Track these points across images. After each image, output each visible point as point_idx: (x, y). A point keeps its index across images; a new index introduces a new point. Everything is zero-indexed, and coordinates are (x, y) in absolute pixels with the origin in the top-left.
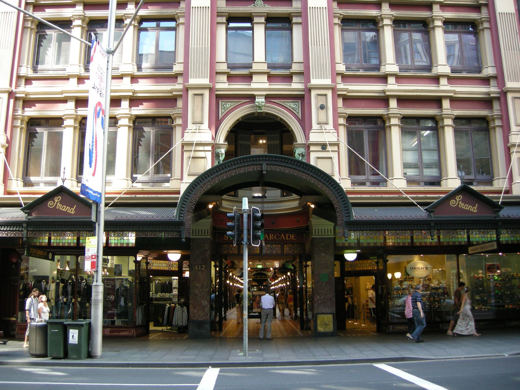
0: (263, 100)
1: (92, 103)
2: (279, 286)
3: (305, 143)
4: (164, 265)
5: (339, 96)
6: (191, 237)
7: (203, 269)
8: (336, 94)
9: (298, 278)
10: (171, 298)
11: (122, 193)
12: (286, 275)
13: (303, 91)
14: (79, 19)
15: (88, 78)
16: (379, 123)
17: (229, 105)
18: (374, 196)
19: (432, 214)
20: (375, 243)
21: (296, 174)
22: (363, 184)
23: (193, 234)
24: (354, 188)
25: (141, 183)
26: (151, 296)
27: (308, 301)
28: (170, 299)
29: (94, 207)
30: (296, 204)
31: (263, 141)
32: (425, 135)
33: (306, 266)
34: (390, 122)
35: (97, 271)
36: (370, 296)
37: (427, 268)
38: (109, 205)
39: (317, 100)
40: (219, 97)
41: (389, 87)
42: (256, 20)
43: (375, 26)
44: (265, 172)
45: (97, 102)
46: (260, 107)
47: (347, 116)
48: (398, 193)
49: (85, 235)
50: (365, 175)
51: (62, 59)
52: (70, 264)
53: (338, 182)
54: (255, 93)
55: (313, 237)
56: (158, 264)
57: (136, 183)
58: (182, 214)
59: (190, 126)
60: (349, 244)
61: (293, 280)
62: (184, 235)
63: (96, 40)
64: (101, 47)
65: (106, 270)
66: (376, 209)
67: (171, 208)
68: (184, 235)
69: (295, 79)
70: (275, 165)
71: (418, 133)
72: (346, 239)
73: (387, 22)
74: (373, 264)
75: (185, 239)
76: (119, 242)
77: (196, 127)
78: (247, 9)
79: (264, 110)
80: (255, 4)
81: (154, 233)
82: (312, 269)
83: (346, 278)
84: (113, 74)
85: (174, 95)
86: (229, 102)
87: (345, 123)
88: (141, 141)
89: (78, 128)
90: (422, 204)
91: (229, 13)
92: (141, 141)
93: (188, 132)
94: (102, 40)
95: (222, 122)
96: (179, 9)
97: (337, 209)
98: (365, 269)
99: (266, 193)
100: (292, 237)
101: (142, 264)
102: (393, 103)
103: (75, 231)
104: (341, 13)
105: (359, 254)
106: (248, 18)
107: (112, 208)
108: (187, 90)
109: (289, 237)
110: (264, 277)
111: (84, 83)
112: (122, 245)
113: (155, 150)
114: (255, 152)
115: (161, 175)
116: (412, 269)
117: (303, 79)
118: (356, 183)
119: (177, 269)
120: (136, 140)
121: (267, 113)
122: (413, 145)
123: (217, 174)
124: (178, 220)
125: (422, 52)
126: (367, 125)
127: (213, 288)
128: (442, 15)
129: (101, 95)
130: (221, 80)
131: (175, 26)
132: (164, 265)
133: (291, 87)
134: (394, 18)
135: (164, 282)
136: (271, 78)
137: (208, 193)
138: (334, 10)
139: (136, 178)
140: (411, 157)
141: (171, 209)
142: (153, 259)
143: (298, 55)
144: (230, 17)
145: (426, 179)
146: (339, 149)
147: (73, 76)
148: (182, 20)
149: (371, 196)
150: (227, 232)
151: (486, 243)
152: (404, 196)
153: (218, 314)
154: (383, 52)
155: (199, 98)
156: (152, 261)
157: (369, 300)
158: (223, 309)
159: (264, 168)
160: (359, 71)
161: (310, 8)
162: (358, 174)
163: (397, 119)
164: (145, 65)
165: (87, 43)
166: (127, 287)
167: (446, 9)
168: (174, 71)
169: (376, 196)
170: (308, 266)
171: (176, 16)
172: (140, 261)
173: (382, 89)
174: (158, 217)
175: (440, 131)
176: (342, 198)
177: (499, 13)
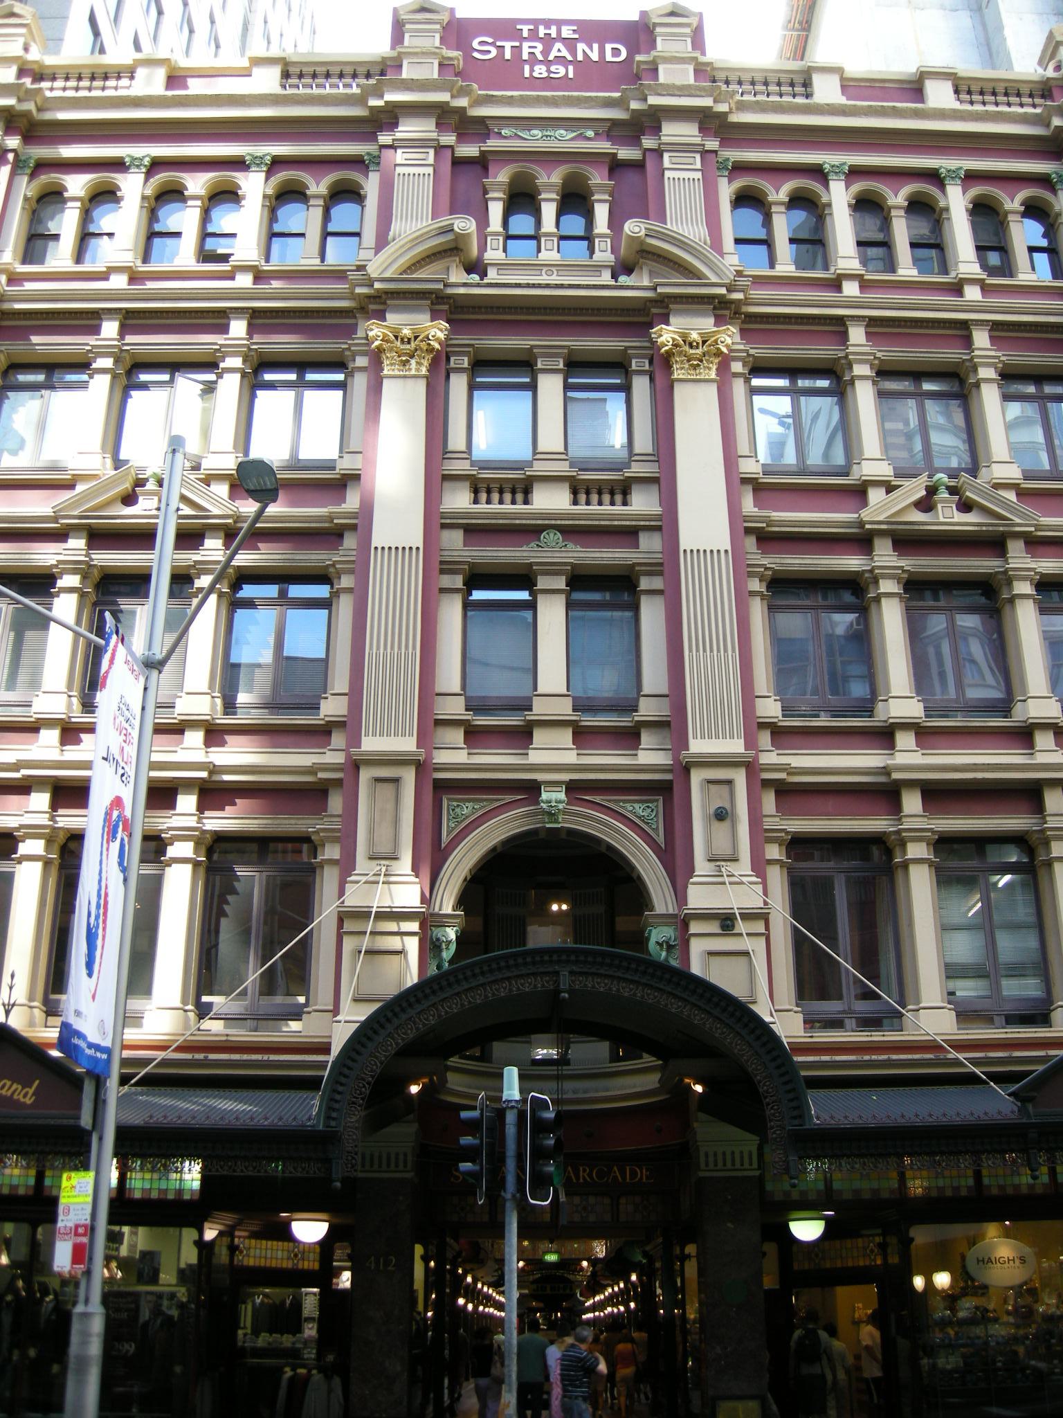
0: (562, 796)
1: (99, 799)
2: (606, 1312)
3: (676, 912)
4: (280, 1253)
5: (766, 783)
6: (360, 1175)
7: (390, 1268)
8: (759, 781)
9: (661, 1287)
10: (299, 1350)
11: (170, 1047)
12: (627, 1281)
13: (670, 771)
14: (74, 572)
15: (91, 729)
16: (875, 851)
17: (468, 809)
18: (867, 1058)
19: (1030, 1107)
20: (875, 1192)
21: (650, 1001)
22: (835, 1024)
23: (363, 1166)
24: (811, 1037)
25: (222, 1022)
26: (240, 1344)
27: (690, 1359)
28: (293, 1355)
29: (88, 1088)
30: (651, 1081)
31: (560, 907)
32: (1001, 884)
33: (684, 1258)
34: (904, 852)
35: (88, 1273)
36: (866, 1341)
37: (1023, 1260)
38: (133, 1082)
40: (442, 787)
41: (900, 759)
42: (543, 582)
43: (858, 598)
44: (567, 995)
45: (112, 797)
46: (554, 814)
47: (790, 837)
48: (933, 1046)
49: (60, 1166)
50: (840, 998)
51: (23, 677)
52: (13, 1245)
53: (767, 1019)
54: (540, 777)
55: (701, 1174)
56: (264, 1252)
57: (211, 1019)
58: (334, 1110)
59: (362, 864)
60: (803, 1193)
61: (645, 1296)
62: (339, 1172)
63: (117, 633)
64: (130, 652)
65: (114, 1265)
66: (874, 1096)
67: (304, 1092)
68: (339, 1172)
69: (646, 738)
70: (593, 974)
71: (981, 881)
72: (793, 1181)
74: (872, 1251)
75: (341, 1183)
76: (155, 1185)
77: (379, 868)
78: (518, 554)
79: (564, 823)
80: (539, 540)
81: (254, 1164)
82: (699, 1263)
83: (794, 1291)
84: (157, 721)
85: (320, 779)
86: (469, 800)
87: (783, 858)
88: (228, 903)
89: (57, 863)
90: (999, 1078)
91: (472, 565)
92: (228, 903)
93: (357, 882)
94: (132, 628)
95: (450, 854)
96: (341, 553)
97: (766, 1098)
98: (850, 1264)
99: (568, 1048)
100: (643, 1174)
101: (217, 1249)
102: (912, 803)
103: (33, 1153)
105: (829, 1223)
106: (523, 578)
107: (139, 1088)
108: (355, 765)
109: (633, 1174)
111: (78, 741)
112: (161, 1197)
113: (265, 923)
114: (541, 936)
115: (279, 999)
116: (981, 1263)
117: (668, 741)
118: (819, 1022)
119: (317, 1266)
120: (212, 897)
121: (571, 832)
122: (970, 914)
123: (434, 999)
124: (324, 1126)
125: (985, 663)
126: (844, 860)
127: (417, 1323)
128: (1033, 565)
129: (124, 778)
130: (447, 740)
131: (328, 595)
132: (280, 1253)
133: (637, 760)
134: (905, 576)
135: (278, 1302)
136: (583, 736)
137: (408, 1051)
139: (210, 1005)
140: (965, 948)
141: (304, 1094)
142: (249, 1237)
143: (654, 676)
144: (473, 574)
145: (1009, 1008)
146: (767, 928)
147: (50, 723)
148: (346, 581)
149: (859, 1058)
150: (460, 1165)
152: (950, 1056)
153: (432, 1395)
154: (879, 666)
155: (387, 790)
156: (247, 1241)
157: (864, 1354)
158: (446, 1381)
159: (564, 985)
160: (818, 716)
161: (685, 551)
162: (823, 995)
163: (924, 845)
164: (243, 698)
165: (93, 637)
166: (171, 1318)
167: (1041, 549)
168: (322, 716)
169: (874, 1057)
170: (689, 1256)
171: (332, 570)
172: (213, 1242)
173: (882, 765)
174: (266, 1119)
175: (1042, 873)
176: (778, 1067)
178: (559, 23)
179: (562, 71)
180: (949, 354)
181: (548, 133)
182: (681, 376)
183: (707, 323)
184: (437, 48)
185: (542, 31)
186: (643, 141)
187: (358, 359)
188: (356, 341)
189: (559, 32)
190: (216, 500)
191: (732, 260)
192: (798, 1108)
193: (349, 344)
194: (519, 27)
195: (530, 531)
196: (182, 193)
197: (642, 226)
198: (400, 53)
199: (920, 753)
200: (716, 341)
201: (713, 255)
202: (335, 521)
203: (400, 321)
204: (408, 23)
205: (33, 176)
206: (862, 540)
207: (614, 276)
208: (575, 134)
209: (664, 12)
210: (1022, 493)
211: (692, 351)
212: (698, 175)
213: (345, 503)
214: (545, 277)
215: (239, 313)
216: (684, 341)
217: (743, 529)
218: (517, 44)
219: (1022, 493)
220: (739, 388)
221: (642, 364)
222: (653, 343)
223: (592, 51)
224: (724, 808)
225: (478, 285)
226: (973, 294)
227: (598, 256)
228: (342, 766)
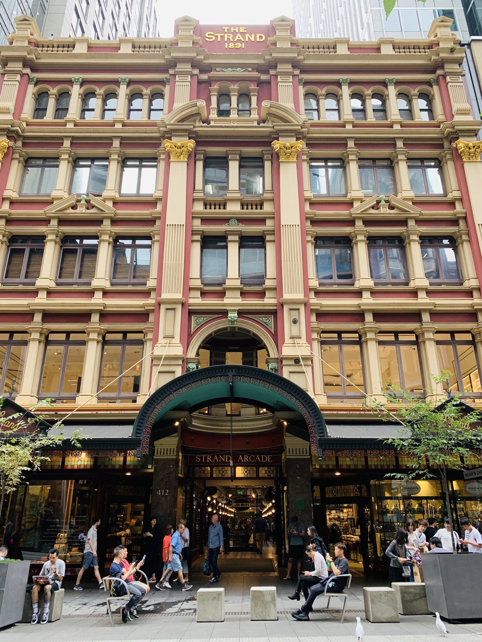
0: (236, 315)
5: (312, 311)
13: (276, 306)
14: (52, 234)
17: (202, 319)
39: (290, 315)
40: (191, 313)
41: (363, 301)
54: (228, 308)
59: (161, 340)
69: (268, 294)
73: (359, 238)
79: (236, 325)
86: (382, 214)
104: (112, 231)
109: (264, 458)
110: (246, 505)
121: (239, 328)
136: (243, 294)
138: (307, 228)
143: (271, 272)
151: (478, 468)
161: (283, 225)
171: (151, 234)
178: (239, 27)
179: (240, 45)
183: (293, 140)
185: (232, 30)
187: (161, 155)
189: (239, 30)
190: (108, 207)
191: (303, 117)
192: (322, 429)
195: (226, 220)
196: (94, 93)
201: (296, 114)
202: (153, 215)
205: (36, 85)
206: (351, 222)
207: (259, 124)
208: (244, 70)
209: (279, 20)
217: (304, 217)
218: (223, 35)
220: (305, 166)
222: (273, 148)
223: (248, 37)
225: (206, 127)
227: (252, 116)
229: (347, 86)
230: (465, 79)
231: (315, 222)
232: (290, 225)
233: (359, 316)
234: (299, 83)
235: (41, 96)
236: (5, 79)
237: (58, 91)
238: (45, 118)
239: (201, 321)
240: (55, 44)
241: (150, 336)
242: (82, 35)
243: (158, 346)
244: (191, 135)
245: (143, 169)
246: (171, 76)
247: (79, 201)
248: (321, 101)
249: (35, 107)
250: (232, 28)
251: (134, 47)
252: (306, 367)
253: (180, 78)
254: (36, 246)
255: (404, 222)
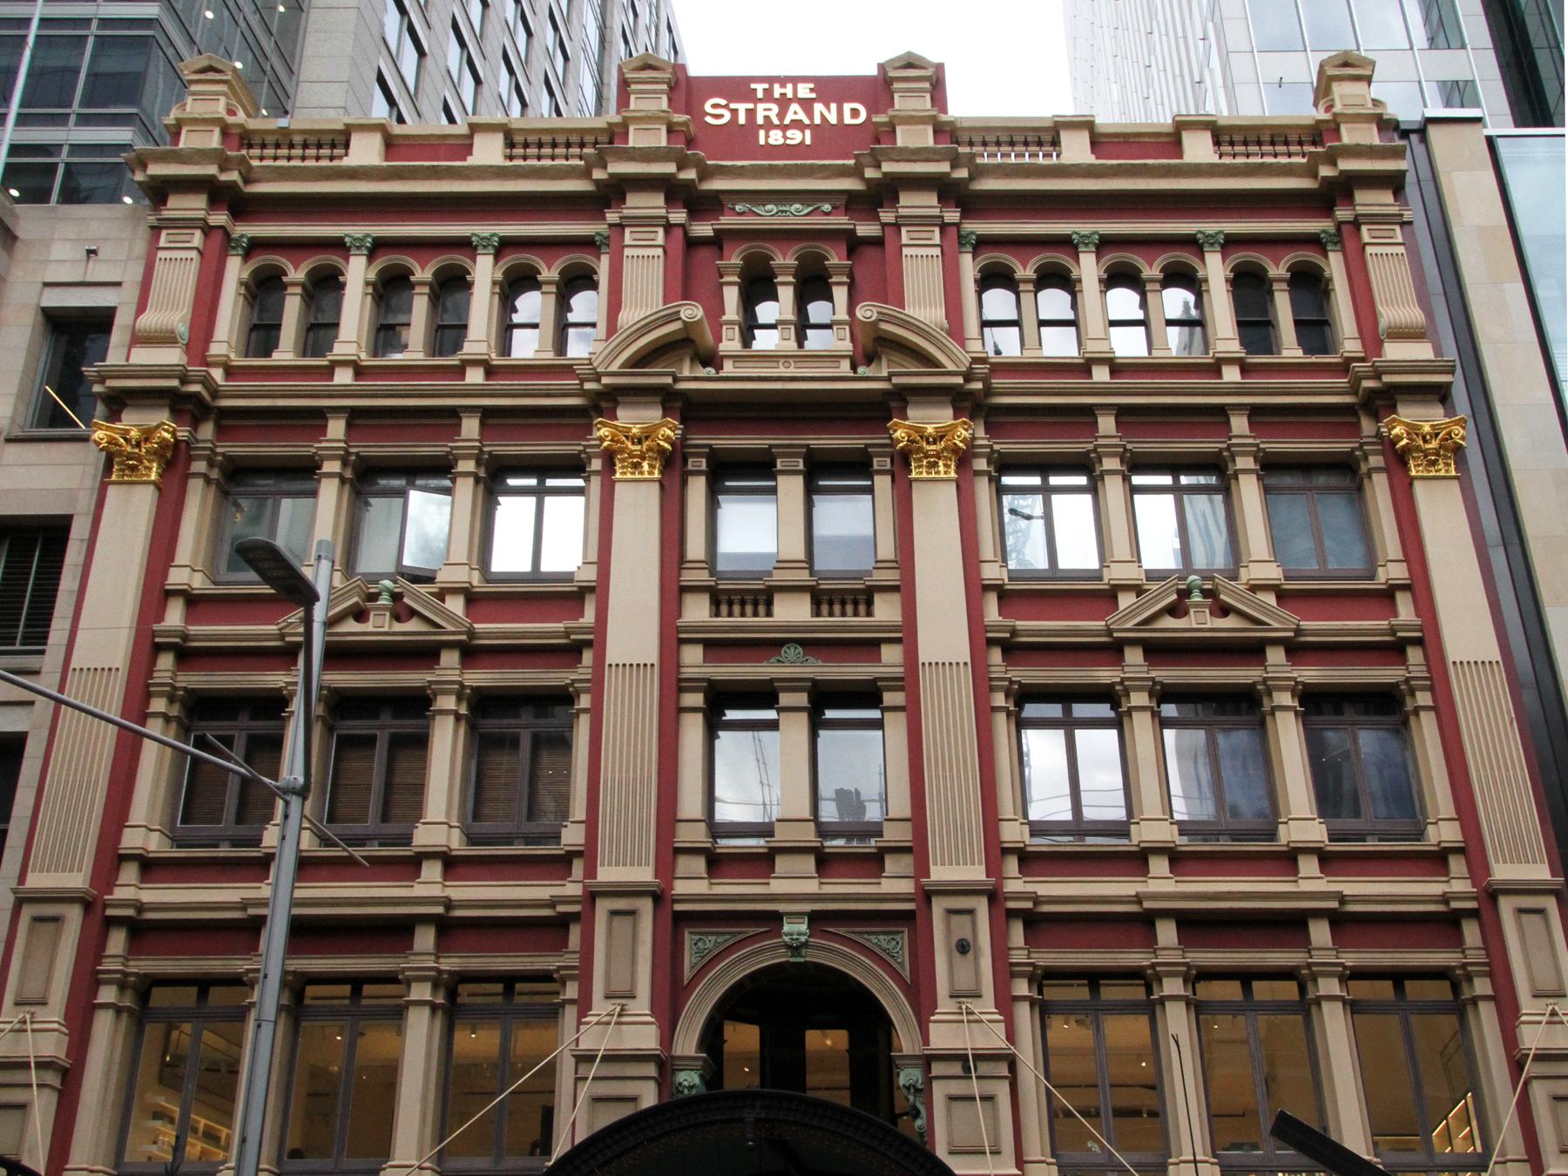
0: (804, 927)
5: (1012, 914)
40: (682, 920)
41: (1153, 886)
42: (785, 699)
69: (891, 864)
80: (780, 655)
86: (708, 934)
104: (1013, 679)
108: (591, 897)
128: (1295, 675)
155: (622, 924)
161: (923, 664)
177: (1454, 663)
178: (795, 80)
180: (1206, 445)
181: (784, 208)
182: (1420, 474)
184: (664, 111)
185: (777, 91)
186: (881, 214)
188: (324, 445)
189: (795, 91)
193: (584, 446)
194: (753, 86)
195: (769, 646)
197: (874, 309)
198: (625, 118)
199: (1173, 881)
200: (1449, 434)
203: (632, 418)
204: (635, 83)
206: (1113, 650)
207: (854, 368)
208: (810, 209)
210: (1283, 596)
211: (929, 448)
212: (937, 251)
213: (583, 617)
214: (782, 369)
215: (469, 412)
216: (921, 437)
217: (981, 640)
218: (751, 106)
219: (1283, 596)
220: (983, 489)
221: (884, 463)
223: (821, 113)
224: (966, 940)
226: (1231, 375)
228: (580, 899)
229: (1094, 255)
230: (1413, 234)
231: (1013, 649)
232: (944, 664)
233: (1140, 923)
234: (961, 244)
235: (264, 288)
236: (162, 243)
237: (310, 274)
238: (275, 355)
239: (709, 945)
240: (297, 139)
241: (572, 991)
242: (522, 114)
243: (588, 1023)
244: (669, 399)
245: (550, 501)
246: (613, 228)
247: (374, 597)
248: (1150, 296)
249: (251, 320)
250: (777, 87)
251: (510, 144)
252: (982, 1081)
253: (171, 238)
254: (407, 726)
255: (1251, 651)
